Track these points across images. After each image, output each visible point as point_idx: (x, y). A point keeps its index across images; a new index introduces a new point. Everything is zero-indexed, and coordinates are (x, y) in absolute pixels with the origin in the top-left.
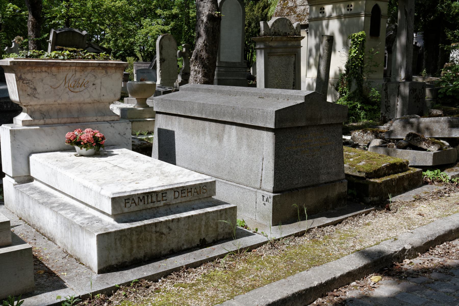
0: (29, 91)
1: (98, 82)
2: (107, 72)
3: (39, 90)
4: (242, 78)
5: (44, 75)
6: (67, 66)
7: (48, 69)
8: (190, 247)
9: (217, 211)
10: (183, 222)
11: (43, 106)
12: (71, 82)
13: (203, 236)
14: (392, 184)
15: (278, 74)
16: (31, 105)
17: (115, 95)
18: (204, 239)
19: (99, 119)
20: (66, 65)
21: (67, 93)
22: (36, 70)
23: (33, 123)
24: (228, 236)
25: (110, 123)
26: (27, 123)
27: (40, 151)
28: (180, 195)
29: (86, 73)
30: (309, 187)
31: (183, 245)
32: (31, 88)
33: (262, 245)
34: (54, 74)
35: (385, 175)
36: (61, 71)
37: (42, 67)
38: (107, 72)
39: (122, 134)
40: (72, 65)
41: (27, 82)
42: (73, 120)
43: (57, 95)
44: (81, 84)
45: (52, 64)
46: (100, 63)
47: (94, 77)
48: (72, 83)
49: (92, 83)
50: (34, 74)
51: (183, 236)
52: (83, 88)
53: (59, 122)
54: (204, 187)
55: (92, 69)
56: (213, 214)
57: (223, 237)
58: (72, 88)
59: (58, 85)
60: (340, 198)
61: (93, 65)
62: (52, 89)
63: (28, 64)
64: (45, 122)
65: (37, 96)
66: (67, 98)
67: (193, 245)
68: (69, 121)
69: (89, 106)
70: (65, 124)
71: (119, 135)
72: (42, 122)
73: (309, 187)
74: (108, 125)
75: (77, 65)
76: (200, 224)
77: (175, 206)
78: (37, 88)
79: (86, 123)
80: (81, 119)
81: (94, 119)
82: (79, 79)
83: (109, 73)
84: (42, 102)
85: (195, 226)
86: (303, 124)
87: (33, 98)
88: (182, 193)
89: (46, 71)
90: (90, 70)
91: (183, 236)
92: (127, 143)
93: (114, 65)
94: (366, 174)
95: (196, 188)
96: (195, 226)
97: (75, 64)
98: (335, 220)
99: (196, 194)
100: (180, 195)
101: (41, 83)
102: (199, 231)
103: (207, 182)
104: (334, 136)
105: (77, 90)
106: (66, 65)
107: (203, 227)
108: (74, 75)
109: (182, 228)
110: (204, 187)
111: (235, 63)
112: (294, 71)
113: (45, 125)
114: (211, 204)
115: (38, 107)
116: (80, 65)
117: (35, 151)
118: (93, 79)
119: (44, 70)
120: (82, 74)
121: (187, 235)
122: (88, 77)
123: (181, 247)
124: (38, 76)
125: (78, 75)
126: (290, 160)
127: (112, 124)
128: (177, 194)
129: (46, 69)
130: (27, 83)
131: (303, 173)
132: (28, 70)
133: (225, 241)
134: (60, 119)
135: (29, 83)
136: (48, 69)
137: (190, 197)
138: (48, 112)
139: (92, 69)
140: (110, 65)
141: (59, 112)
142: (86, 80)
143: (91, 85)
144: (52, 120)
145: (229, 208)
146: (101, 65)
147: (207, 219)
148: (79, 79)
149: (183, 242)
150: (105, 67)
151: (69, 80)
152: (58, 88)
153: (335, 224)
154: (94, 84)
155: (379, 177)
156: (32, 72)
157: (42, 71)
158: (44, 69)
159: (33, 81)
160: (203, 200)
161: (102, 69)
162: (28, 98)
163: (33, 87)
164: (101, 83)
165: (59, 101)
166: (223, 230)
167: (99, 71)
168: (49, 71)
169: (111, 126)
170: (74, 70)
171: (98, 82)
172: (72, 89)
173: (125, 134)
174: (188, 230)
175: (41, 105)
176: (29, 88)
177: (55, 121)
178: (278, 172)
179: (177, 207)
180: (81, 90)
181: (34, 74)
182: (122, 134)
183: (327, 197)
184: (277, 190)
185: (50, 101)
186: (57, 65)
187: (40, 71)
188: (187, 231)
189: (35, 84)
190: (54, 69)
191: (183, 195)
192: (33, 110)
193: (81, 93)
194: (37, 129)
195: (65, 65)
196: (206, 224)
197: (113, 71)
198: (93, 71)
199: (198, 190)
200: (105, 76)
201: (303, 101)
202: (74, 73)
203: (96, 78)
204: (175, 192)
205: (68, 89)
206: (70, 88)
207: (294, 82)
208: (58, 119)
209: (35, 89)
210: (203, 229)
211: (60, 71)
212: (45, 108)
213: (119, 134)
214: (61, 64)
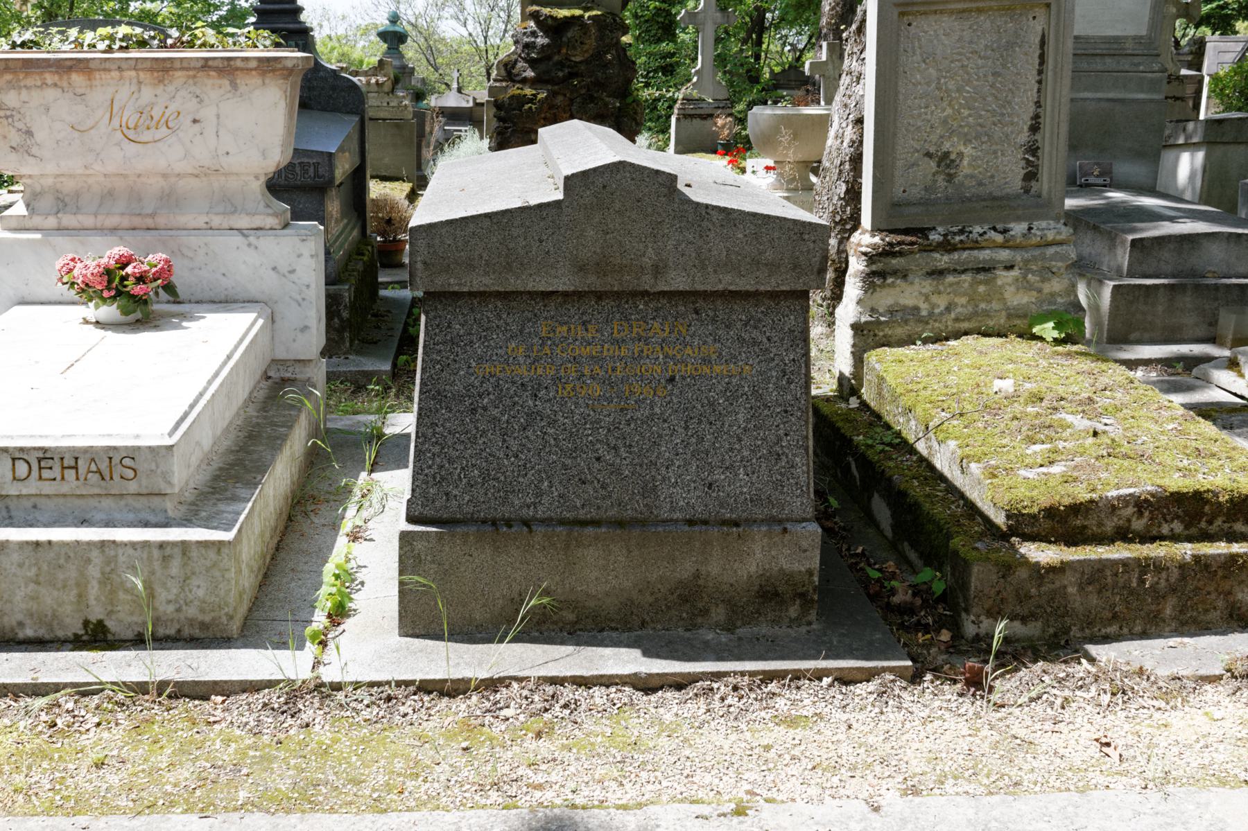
0: (15, 138)
1: (208, 113)
2: (234, 86)
3: (40, 136)
4: (1142, 96)
5: (51, 94)
6: (110, 70)
7: (61, 79)
8: (47, 637)
9: (146, 544)
10: (15, 557)
11: (63, 179)
12: (126, 114)
13: (96, 614)
14: (1142, 582)
15: (951, 85)
16: (30, 176)
17: (264, 154)
18: (100, 623)
19: (216, 221)
20: (107, 65)
21: (118, 144)
22: (29, 82)
23: (29, 224)
24: (197, 633)
25: (244, 235)
26: (14, 224)
27: (43, 299)
28: (35, 473)
29: (171, 88)
30: (595, 523)
31: (21, 624)
32: (19, 130)
33: (258, 691)
34: (80, 91)
35: (1123, 535)
36: (97, 82)
37: (42, 73)
38: (234, 86)
39: (285, 270)
40: (124, 65)
41: (8, 113)
42: (137, 221)
43: (91, 150)
44: (156, 118)
45: (68, 63)
46: (207, 59)
47: (195, 100)
48: (130, 116)
49: (190, 118)
50: (24, 92)
51: (18, 598)
52: (164, 129)
53: (99, 225)
54: (127, 462)
55: (189, 77)
56: (131, 551)
57: (179, 631)
58: (132, 131)
59: (89, 123)
60: (770, 595)
61: (185, 64)
62: (76, 134)
63: (178, 65)
64: (59, 223)
65: (34, 150)
66: (115, 160)
67: (60, 634)
68: (126, 222)
69: (194, 182)
70: (114, 230)
71: (272, 273)
72: (51, 222)
73: (595, 523)
74: (237, 239)
75: (139, 66)
76: (82, 574)
77: (28, 504)
78: (33, 129)
79: (170, 233)
80: (161, 221)
81: (201, 221)
82: (152, 105)
83: (242, 88)
84: (50, 168)
85: (61, 576)
86: (563, 283)
87: (26, 156)
88: (40, 468)
89: (55, 85)
90: (182, 80)
91: (18, 598)
92: (299, 298)
93: (253, 64)
94: (1008, 517)
95: (93, 460)
96: (61, 576)
97: (133, 63)
98: (655, 671)
99: (94, 478)
100: (35, 473)
101: (44, 117)
102: (80, 596)
103: (139, 448)
104: (755, 343)
105: (146, 136)
106: (107, 65)
107: (95, 583)
108: (136, 95)
109: (15, 575)
110: (127, 462)
111: (1116, 40)
112: (1040, 72)
113: (60, 229)
114: (152, 519)
115: (50, 181)
116: (148, 64)
117: (29, 299)
118: (192, 104)
119: (49, 81)
120: (160, 90)
121: (32, 598)
122: (176, 98)
123: (12, 630)
124: (36, 98)
125: (147, 94)
126: (495, 412)
127: (252, 239)
128: (22, 469)
129: (56, 78)
130: (7, 117)
131: (565, 467)
132: (9, 82)
133: (170, 644)
134: (100, 218)
135: (12, 116)
136: (61, 79)
137: (71, 484)
138: (77, 195)
139: (189, 77)
140: (239, 64)
141: (109, 195)
142: (173, 107)
143: (188, 122)
144: (80, 217)
145: (198, 542)
146: (210, 63)
147: (108, 563)
148: (152, 105)
149: (20, 617)
150: (228, 69)
151: (123, 108)
152: (92, 131)
153: (648, 685)
154: (195, 121)
155: (1072, 540)
156: (20, 88)
157: (44, 84)
158: (50, 78)
159: (22, 111)
160: (130, 500)
161: (220, 77)
162: (13, 156)
163: (24, 129)
164: (218, 116)
165: (97, 167)
166: (178, 610)
167: (210, 82)
168: (65, 84)
169: (249, 245)
170: (135, 81)
171: (208, 113)
172: (129, 134)
173: (292, 272)
174: (38, 583)
175: (58, 176)
176: (13, 131)
177: (89, 221)
178: (436, 449)
179: (35, 507)
180: (158, 135)
181: (24, 92)
182: (284, 269)
183: (697, 575)
184: (429, 512)
185: (74, 165)
186: (81, 66)
187: (39, 83)
188: (32, 586)
189: (28, 119)
190: (76, 78)
191: (46, 474)
192: (38, 189)
193: (160, 144)
194: (33, 240)
195: (103, 66)
196: (105, 579)
197: (255, 80)
198: (191, 81)
199: (104, 466)
200: (230, 95)
201: (559, 196)
202: (134, 88)
203: (201, 102)
204: (14, 459)
205: (119, 135)
206: (126, 131)
207: (1036, 117)
208: (96, 215)
209: (29, 133)
210: (94, 590)
211: (94, 83)
212: (69, 186)
213: (274, 269)
214: (92, 65)
